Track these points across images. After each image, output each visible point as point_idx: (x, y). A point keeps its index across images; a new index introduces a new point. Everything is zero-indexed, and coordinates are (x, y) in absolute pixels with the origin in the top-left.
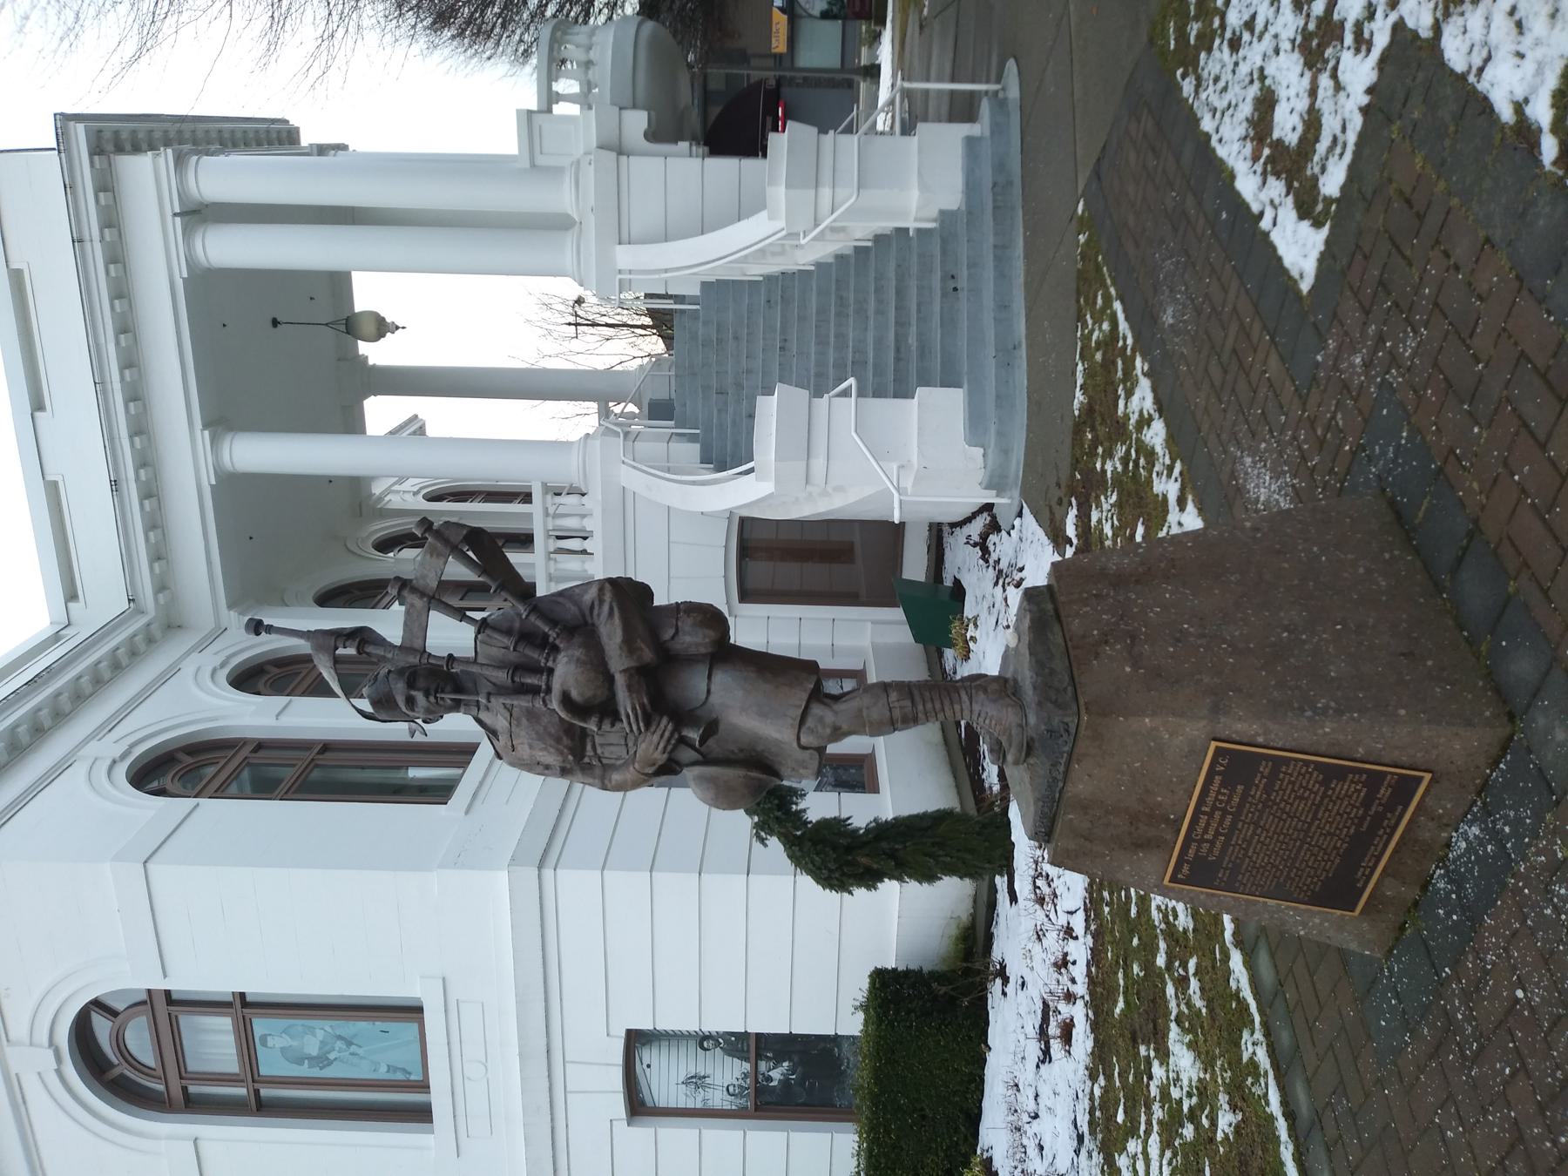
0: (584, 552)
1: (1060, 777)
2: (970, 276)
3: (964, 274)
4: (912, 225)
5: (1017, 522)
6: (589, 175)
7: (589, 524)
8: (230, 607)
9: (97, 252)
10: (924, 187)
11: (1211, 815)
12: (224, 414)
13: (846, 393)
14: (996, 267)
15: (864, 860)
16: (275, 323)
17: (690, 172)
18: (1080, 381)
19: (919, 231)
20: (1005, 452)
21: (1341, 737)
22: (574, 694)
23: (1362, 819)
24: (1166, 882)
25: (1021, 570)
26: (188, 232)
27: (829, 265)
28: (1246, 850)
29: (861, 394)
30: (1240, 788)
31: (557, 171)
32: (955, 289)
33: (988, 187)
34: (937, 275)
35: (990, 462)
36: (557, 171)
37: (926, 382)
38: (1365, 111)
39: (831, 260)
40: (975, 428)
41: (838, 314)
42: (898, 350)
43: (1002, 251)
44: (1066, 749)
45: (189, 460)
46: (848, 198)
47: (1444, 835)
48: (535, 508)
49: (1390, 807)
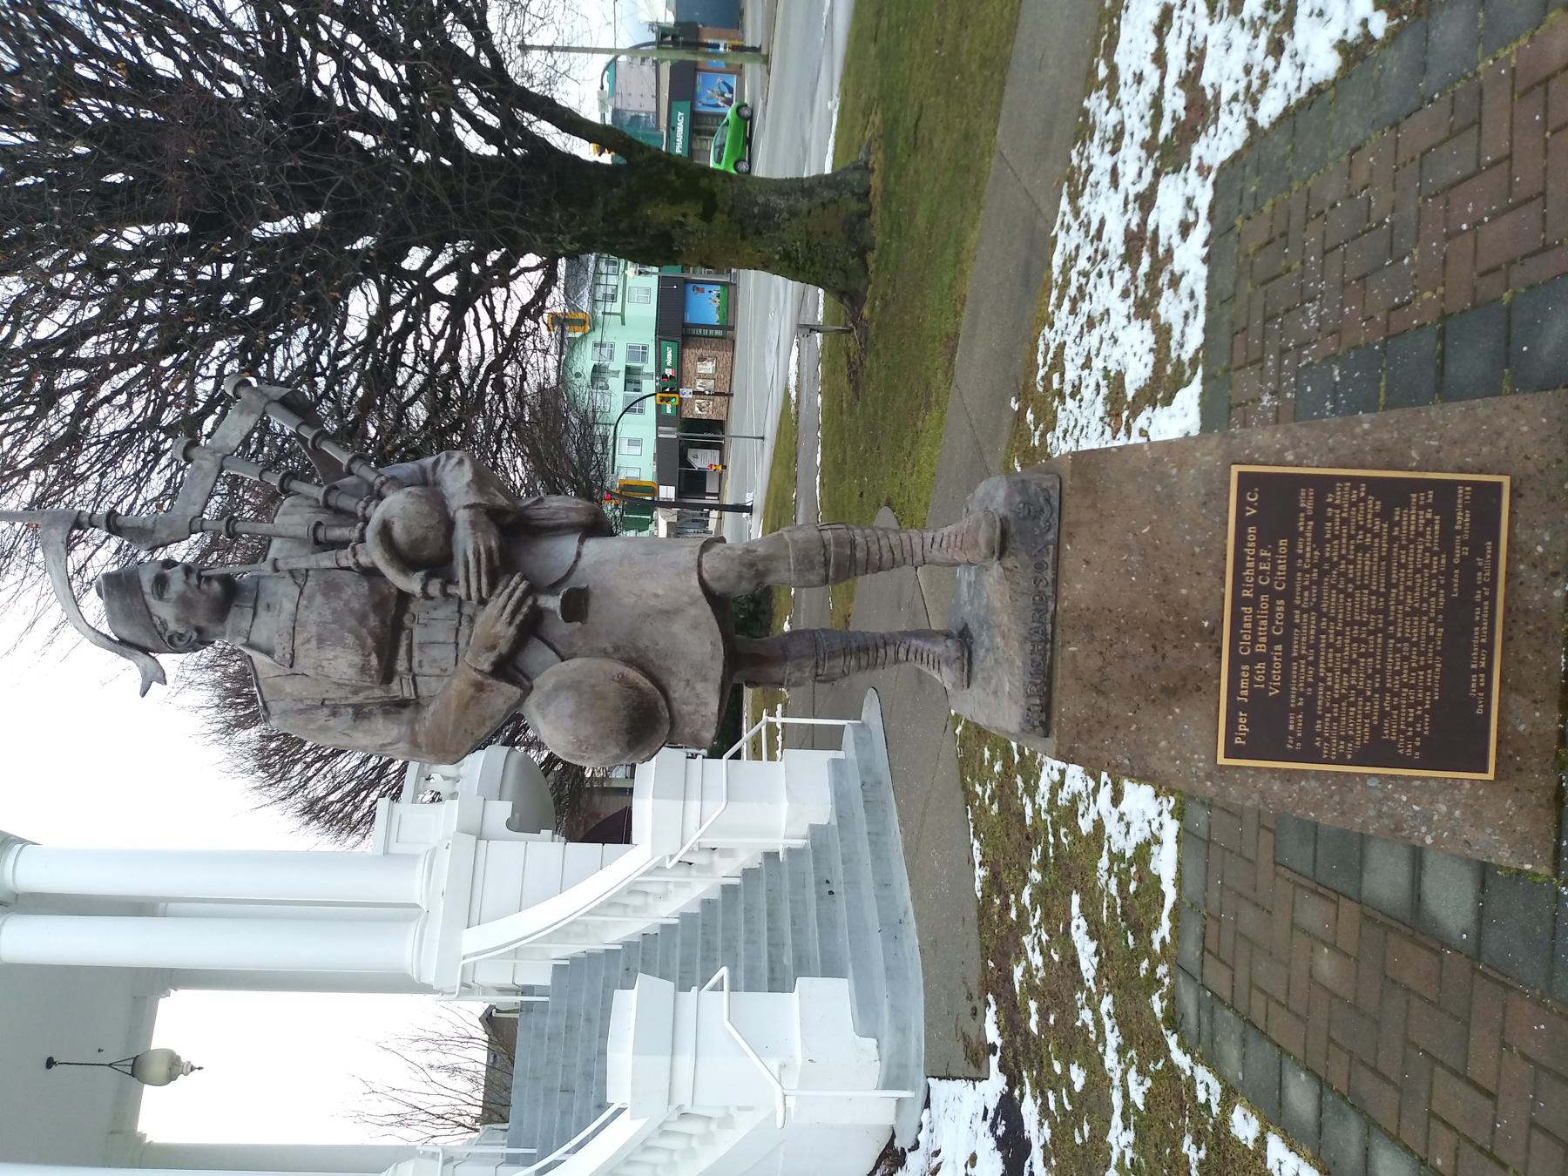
1: (1049, 591)
2: (845, 871)
3: (839, 875)
4: (779, 844)
6: (444, 860)
10: (792, 798)
11: (1254, 602)
13: (718, 987)
14: (872, 852)
16: (50, 1063)
17: (548, 848)
18: (978, 858)
19: (789, 851)
20: (902, 1030)
21: (1386, 436)
22: (398, 531)
23: (1448, 574)
24: (1221, 760)
25: (937, 1153)
27: (695, 915)
28: (1315, 664)
29: (733, 989)
30: (1283, 543)
31: (413, 858)
32: (831, 893)
33: (857, 799)
34: (811, 880)
35: (885, 1056)
36: (413, 858)
37: (802, 968)
39: (696, 910)
41: (704, 959)
42: (772, 970)
44: (1051, 536)
46: (715, 808)
49: (1478, 550)
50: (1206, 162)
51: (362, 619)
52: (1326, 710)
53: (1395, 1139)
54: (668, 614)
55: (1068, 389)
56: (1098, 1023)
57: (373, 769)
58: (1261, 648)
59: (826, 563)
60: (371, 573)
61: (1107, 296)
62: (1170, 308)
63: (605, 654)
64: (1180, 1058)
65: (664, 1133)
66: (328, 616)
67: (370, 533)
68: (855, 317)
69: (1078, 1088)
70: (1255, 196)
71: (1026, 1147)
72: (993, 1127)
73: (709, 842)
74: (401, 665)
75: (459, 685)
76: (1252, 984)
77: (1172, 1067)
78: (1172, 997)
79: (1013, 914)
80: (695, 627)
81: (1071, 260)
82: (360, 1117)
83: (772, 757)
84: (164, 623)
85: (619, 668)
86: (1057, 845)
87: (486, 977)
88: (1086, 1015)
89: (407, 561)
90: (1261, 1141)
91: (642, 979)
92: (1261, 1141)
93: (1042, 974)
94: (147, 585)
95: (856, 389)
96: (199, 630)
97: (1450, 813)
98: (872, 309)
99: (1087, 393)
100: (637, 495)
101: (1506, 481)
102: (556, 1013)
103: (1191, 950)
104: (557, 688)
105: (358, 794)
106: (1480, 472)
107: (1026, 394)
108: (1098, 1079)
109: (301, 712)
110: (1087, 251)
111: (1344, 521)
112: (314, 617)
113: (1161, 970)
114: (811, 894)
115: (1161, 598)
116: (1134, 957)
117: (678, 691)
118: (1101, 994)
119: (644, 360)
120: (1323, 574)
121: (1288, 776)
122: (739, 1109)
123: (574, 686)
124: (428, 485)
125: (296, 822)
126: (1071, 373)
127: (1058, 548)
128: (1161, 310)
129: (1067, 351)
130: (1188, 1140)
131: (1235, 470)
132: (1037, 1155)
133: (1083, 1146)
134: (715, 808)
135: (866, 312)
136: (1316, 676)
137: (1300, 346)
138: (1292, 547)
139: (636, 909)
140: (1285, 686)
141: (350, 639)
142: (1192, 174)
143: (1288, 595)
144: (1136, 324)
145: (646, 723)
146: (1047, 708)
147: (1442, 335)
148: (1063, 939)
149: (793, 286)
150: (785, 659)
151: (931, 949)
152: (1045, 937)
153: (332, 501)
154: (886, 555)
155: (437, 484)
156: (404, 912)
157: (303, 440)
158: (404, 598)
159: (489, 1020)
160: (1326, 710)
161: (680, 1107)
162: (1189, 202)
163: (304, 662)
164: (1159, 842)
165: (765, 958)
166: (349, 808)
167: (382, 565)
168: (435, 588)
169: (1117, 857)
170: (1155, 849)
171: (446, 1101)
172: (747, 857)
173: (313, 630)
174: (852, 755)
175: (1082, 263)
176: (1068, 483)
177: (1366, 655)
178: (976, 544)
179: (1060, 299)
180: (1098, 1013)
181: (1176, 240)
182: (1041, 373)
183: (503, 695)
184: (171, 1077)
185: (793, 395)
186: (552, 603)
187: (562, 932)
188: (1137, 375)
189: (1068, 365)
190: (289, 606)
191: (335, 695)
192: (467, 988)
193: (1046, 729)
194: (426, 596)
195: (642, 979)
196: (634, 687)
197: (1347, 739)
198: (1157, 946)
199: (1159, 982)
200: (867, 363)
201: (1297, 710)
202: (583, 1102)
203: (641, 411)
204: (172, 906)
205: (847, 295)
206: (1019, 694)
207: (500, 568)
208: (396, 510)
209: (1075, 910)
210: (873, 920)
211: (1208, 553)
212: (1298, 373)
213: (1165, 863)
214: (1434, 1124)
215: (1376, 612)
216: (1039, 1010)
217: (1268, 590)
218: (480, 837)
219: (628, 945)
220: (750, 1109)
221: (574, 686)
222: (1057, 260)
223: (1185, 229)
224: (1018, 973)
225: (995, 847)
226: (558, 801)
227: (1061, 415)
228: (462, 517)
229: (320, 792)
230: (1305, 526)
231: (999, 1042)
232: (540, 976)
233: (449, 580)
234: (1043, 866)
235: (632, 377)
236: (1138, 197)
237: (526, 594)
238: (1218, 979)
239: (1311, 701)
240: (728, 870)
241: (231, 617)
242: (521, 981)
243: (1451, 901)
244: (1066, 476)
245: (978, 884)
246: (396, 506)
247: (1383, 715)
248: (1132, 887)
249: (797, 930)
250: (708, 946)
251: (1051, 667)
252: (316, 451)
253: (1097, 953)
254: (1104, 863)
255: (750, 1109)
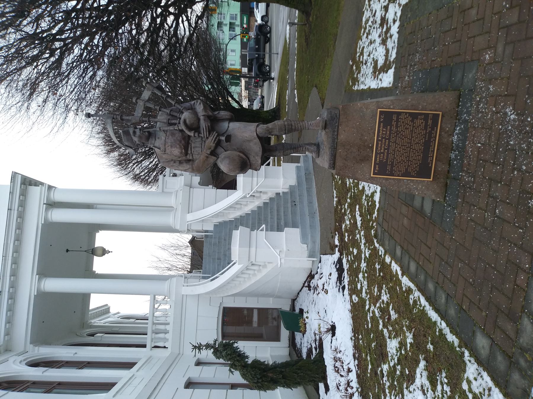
0: (165, 347)
1: (336, 137)
3: (297, 200)
4: (280, 191)
5: (319, 265)
6: (180, 194)
7: (168, 327)
8: (31, 343)
9: (15, 214)
10: (284, 177)
11: (381, 141)
12: (45, 270)
13: (262, 230)
15: (270, 375)
16: (67, 251)
17: (211, 191)
18: (335, 196)
19: (283, 193)
20: (314, 242)
21: (414, 102)
22: (188, 121)
23: (425, 135)
24: (372, 175)
25: (322, 274)
26: (47, 209)
27: (255, 211)
28: (394, 155)
29: (267, 230)
31: (172, 193)
33: (303, 178)
36: (172, 193)
37: (286, 225)
38: (398, 33)
39: (256, 209)
40: (304, 239)
41: (258, 223)
42: (278, 226)
43: (309, 190)
45: (29, 285)
46: (261, 180)
47: (450, 139)
48: (148, 337)
49: (433, 129)
50: (401, 3)
51: (180, 142)
52: (396, 165)
53: (414, 259)
54: (249, 141)
55: (364, 62)
56: (360, 238)
57: (154, 165)
58: (382, 151)
59: (285, 130)
60: (182, 131)
61: (375, 35)
62: (390, 44)
63: (235, 150)
64: (377, 245)
65: (247, 269)
66: (173, 141)
67: (181, 122)
68: (308, 20)
69: (355, 254)
70: (410, 18)
71: (343, 270)
72: (336, 266)
73: (259, 190)
74: (189, 152)
75: (203, 157)
76: (392, 227)
77: (375, 247)
78: (376, 231)
79: (343, 211)
80: (255, 144)
81: (367, 21)
82: (157, 268)
83: (279, 165)
84: (135, 142)
85: (239, 153)
86: (354, 192)
87: (194, 227)
88: (358, 236)
89: (190, 128)
90: (391, 262)
91: (240, 227)
92: (391, 262)
93: (349, 226)
94: (132, 133)
95: (307, 45)
96: (143, 143)
97: (422, 187)
98: (313, 19)
99: (369, 64)
100: (234, 74)
101: (441, 113)
102: (215, 238)
103: (381, 219)
104: (225, 158)
105: (150, 173)
106: (435, 111)
107: (354, 60)
108: (360, 252)
109: (167, 162)
110: (371, 19)
111: (403, 122)
112: (169, 141)
113: (375, 224)
114: (289, 205)
115: (361, 139)
116: (369, 221)
117: (252, 158)
118: (361, 230)
119: (236, 20)
120: (397, 134)
121: (387, 179)
122: (269, 263)
123: (228, 157)
124: (192, 109)
125: (131, 182)
126: (365, 58)
127: (338, 127)
128: (388, 43)
129: (365, 50)
130: (377, 264)
131: (379, 110)
132: (346, 272)
133: (356, 268)
134: (261, 180)
135: (311, 19)
136: (394, 157)
137: (415, 65)
138: (391, 128)
139: (238, 209)
140: (387, 160)
141: (178, 146)
142: (397, 5)
143: (389, 139)
144: (382, 46)
145: (244, 165)
146: (334, 164)
147: (440, 70)
148: (354, 217)
149: (287, 9)
150: (276, 150)
151: (322, 221)
152: (350, 217)
153: (171, 113)
154: (299, 128)
155: (195, 109)
156: (169, 209)
157: (163, 98)
158: (189, 137)
159: (193, 242)
160: (396, 165)
161: (252, 262)
162: (396, 13)
163: (168, 151)
164: (376, 192)
165: (276, 222)
166: (147, 178)
167: (184, 130)
168: (196, 135)
169: (367, 196)
170: (375, 194)
171: (181, 264)
172: (271, 194)
173: (170, 144)
174: (303, 165)
175: (370, 23)
176: (341, 112)
177: (406, 153)
178: (319, 126)
179: (364, 32)
180: (360, 236)
181: (392, 24)
182: (358, 54)
183: (212, 159)
184: (103, 254)
185: (288, 41)
186: (223, 138)
187: (217, 215)
188: (381, 62)
189: (365, 54)
190: (163, 138)
191: (174, 158)
192: (189, 231)
193: (334, 168)
194: (194, 136)
195: (240, 227)
196: (242, 158)
197: (400, 171)
198: (374, 218)
199: (374, 227)
200: (311, 37)
201: (389, 165)
202: (225, 260)
203: (235, 39)
204: (98, 206)
205: (305, 13)
206: (328, 160)
207: (211, 130)
208: (187, 117)
209: (357, 209)
210: (307, 213)
211: (372, 129)
212: (414, 72)
213: (377, 198)
214: (421, 255)
215: (409, 143)
216: (348, 236)
217: (385, 138)
218: (191, 187)
219: (236, 219)
220: (271, 263)
221: (228, 157)
222: (364, 19)
223: (394, 21)
224: (344, 226)
225: (340, 193)
226: (212, 175)
227: (362, 69)
228: (202, 118)
229: (138, 172)
230: (394, 123)
231: (338, 244)
232: (210, 227)
233: (199, 133)
234: (351, 198)
235: (232, 26)
236: (385, 7)
237: (217, 136)
238: (385, 225)
239: (393, 163)
240: (265, 198)
241: (150, 140)
242: (204, 229)
243: (428, 207)
244: (341, 110)
245: (335, 203)
246: (186, 115)
247: (408, 166)
248: (370, 204)
249: (285, 215)
250: (259, 219)
251: (336, 154)
252: (166, 100)
253: (361, 220)
254: (364, 197)
255: (271, 263)
